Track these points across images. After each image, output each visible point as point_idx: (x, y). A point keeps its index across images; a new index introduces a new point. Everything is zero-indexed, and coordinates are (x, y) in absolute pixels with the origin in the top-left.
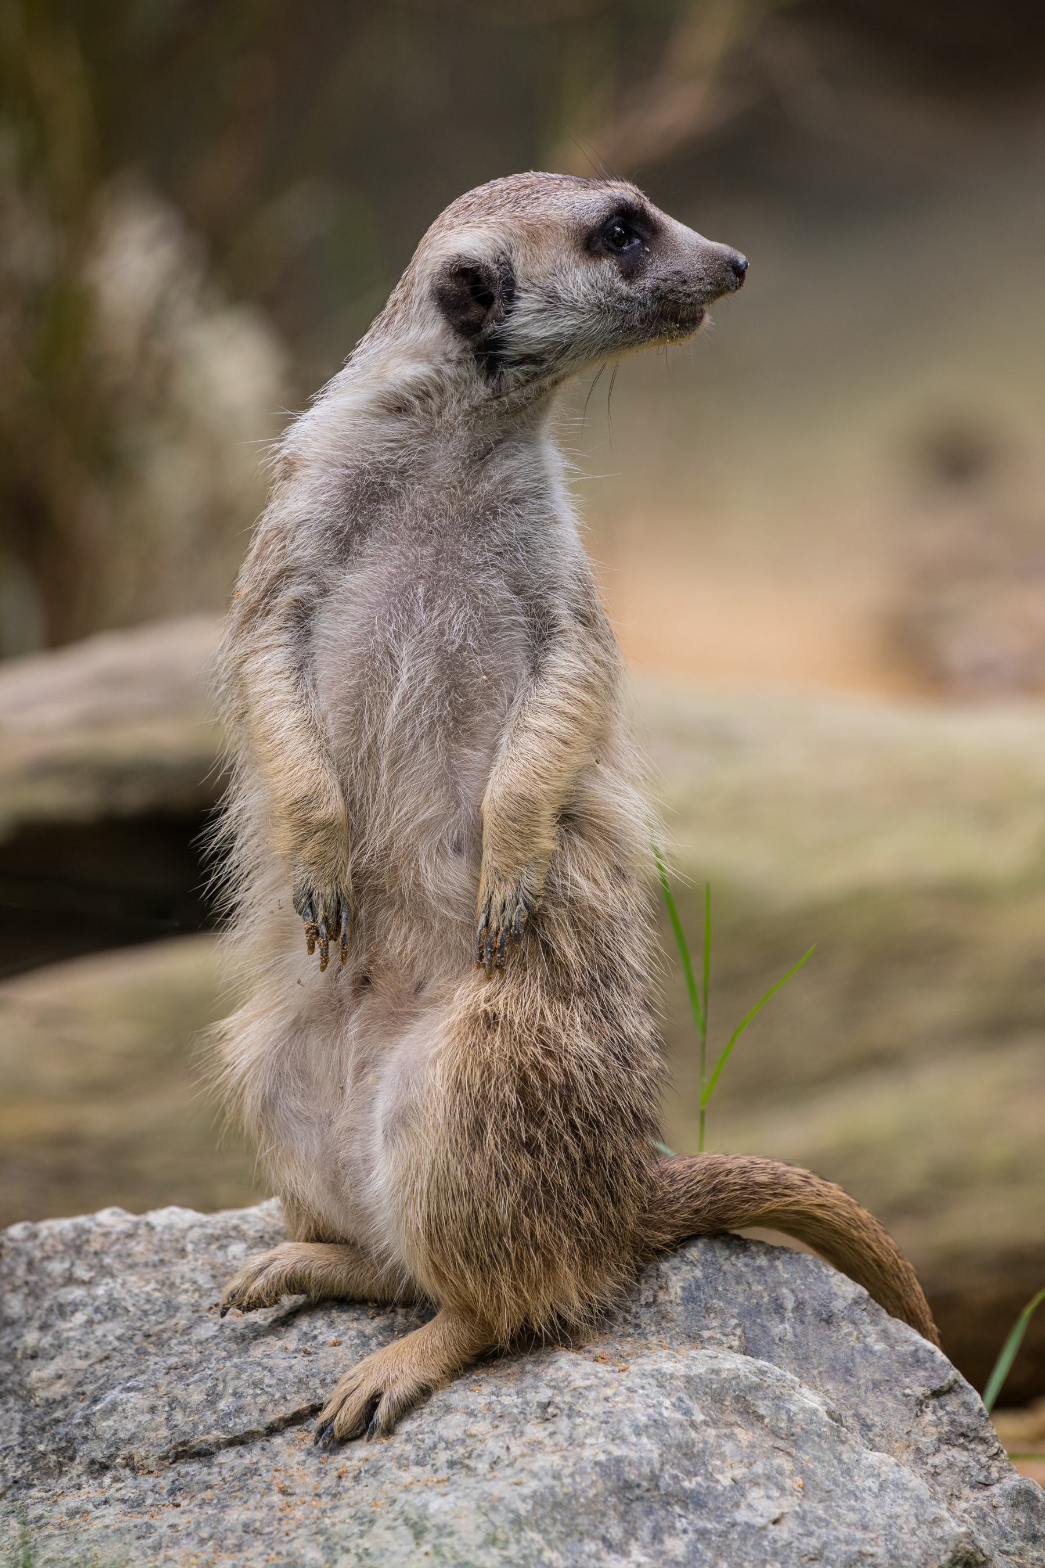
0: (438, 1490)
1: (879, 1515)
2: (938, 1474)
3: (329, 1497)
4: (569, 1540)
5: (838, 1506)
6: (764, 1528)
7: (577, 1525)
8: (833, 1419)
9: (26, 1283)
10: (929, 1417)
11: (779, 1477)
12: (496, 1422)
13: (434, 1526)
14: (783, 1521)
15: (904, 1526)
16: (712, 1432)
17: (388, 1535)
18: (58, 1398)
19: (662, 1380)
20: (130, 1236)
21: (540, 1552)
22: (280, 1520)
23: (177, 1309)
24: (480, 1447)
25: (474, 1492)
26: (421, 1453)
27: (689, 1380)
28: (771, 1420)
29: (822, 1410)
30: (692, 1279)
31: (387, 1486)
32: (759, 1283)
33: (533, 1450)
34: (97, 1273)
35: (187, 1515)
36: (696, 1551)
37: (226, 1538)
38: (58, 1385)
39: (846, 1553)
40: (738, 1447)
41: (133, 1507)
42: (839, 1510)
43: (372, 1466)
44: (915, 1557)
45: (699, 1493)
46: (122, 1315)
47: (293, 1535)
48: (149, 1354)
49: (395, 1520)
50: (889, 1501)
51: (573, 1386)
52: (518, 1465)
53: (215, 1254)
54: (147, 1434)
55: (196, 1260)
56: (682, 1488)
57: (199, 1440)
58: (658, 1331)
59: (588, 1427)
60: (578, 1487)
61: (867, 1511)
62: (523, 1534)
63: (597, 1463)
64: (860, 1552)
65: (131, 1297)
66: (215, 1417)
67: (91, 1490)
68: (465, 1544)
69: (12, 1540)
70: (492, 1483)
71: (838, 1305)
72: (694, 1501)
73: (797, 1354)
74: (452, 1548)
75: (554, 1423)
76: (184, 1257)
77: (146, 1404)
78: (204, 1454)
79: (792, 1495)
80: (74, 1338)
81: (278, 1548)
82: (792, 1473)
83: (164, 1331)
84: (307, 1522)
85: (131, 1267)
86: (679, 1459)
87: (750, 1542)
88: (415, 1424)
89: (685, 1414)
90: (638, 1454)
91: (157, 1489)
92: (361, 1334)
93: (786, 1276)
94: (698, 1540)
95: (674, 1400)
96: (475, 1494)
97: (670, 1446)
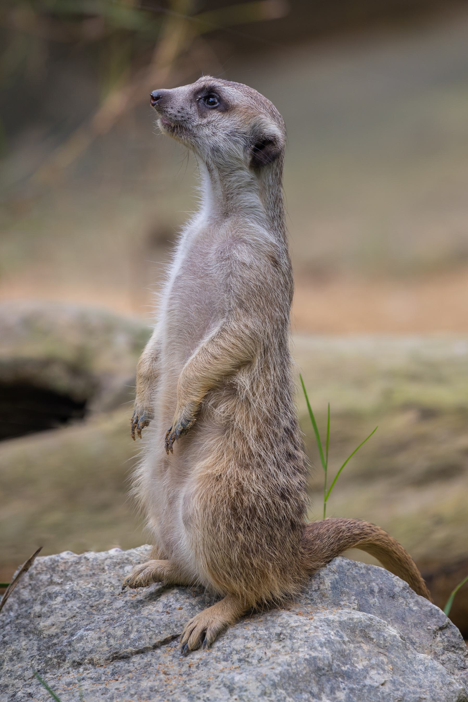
0: (237, 671)
1: (426, 681)
2: (444, 664)
3: (186, 676)
4: (296, 693)
5: (408, 677)
6: (378, 687)
7: (299, 686)
8: (402, 639)
9: (30, 584)
10: (439, 639)
11: (382, 665)
12: (258, 642)
13: (238, 687)
14: (386, 684)
15: (437, 686)
16: (352, 646)
17: (217, 692)
18: (54, 634)
19: (329, 623)
20: (77, 563)
21: (285, 698)
22: (166, 685)
23: (104, 595)
24: (252, 653)
25: (254, 672)
26: (225, 656)
27: (340, 623)
28: (377, 640)
29: (398, 636)
30: (334, 579)
31: (212, 670)
32: (362, 580)
33: (276, 654)
34: (65, 580)
35: (123, 684)
36: (349, 697)
37: (142, 694)
38: (53, 629)
39: (413, 698)
40: (364, 652)
41: (96, 681)
42: (409, 679)
43: (204, 662)
44: (443, 700)
45: (349, 672)
46: (79, 598)
47: (174, 692)
48: (94, 614)
49: (219, 685)
50: (429, 675)
51: (290, 626)
52: (271, 660)
53: (118, 570)
54: (98, 649)
55: (110, 573)
56: (342, 670)
57: (123, 651)
58: (322, 602)
59: (299, 644)
60: (299, 670)
61: (421, 680)
62: (277, 690)
63: (306, 659)
64: (420, 697)
65: (82, 590)
66: (129, 641)
67: (73, 675)
68: (253, 695)
69: (43, 696)
70: (261, 668)
71: (397, 590)
72: (347, 676)
73: (381, 612)
74: (247, 697)
75: (284, 642)
76: (104, 572)
77: (97, 636)
78: (126, 658)
79: (388, 673)
80: (58, 608)
81: (168, 698)
82: (387, 663)
83: (99, 604)
84: (179, 686)
85: (80, 576)
86: (339, 657)
87: (372, 693)
88: (221, 643)
89: (340, 638)
90: (323, 655)
91: (106, 673)
92: (191, 604)
93: (374, 577)
94: (350, 693)
95: (335, 631)
96: (254, 673)
97: (335, 652)
